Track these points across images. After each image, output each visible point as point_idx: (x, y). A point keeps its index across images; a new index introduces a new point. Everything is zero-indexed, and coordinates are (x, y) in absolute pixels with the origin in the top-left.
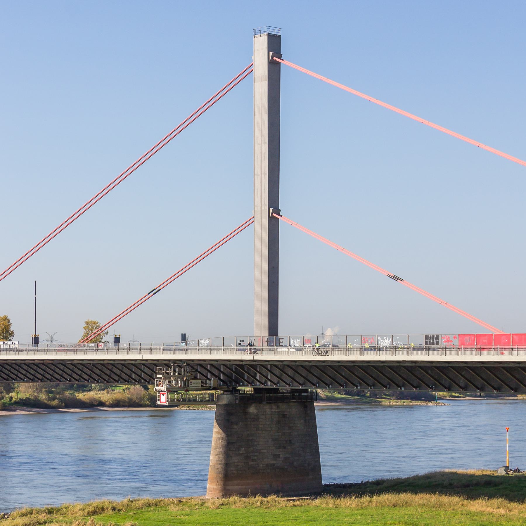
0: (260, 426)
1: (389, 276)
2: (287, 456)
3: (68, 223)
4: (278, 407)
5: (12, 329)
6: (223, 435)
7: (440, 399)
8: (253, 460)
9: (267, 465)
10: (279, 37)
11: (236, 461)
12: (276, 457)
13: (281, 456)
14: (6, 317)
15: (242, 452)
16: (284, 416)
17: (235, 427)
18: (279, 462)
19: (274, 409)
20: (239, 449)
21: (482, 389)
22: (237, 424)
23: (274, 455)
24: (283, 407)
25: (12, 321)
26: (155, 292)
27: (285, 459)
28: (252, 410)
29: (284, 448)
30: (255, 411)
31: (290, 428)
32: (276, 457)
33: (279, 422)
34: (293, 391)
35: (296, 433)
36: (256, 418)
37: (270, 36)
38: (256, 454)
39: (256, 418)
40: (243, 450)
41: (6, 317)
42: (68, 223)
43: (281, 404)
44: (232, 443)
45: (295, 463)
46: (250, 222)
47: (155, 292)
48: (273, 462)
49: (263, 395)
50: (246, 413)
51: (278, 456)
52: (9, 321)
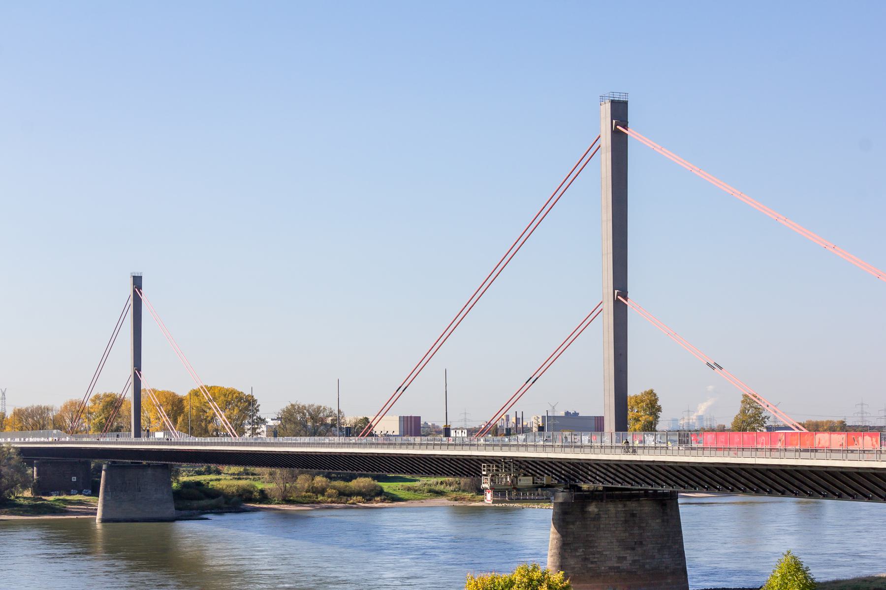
0: (602, 526)
1: (137, 282)
2: (636, 558)
3: (468, 307)
4: (625, 506)
5: (659, 403)
6: (558, 536)
7: (394, 499)
8: (592, 563)
9: (610, 568)
10: (625, 103)
11: (572, 563)
12: (621, 559)
13: (628, 558)
14: (652, 391)
15: (578, 554)
16: (633, 515)
17: (571, 526)
18: (625, 565)
19: (620, 507)
20: (576, 550)
21: (732, 490)
22: (573, 523)
23: (619, 558)
24: (632, 505)
25: (658, 395)
26: (532, 380)
27: (634, 561)
28: (592, 508)
29: (633, 549)
30: (596, 510)
31: (640, 527)
32: (621, 559)
33: (626, 521)
34: (606, 489)
35: (649, 534)
36: (597, 517)
37: (613, 102)
38: (596, 556)
39: (597, 517)
40: (580, 552)
41: (652, 391)
42: (468, 307)
43: (628, 503)
44: (568, 544)
45: (647, 566)
46: (596, 312)
47: (532, 380)
48: (616, 565)
49: (609, 495)
50: (583, 512)
51: (625, 558)
52: (655, 395)
